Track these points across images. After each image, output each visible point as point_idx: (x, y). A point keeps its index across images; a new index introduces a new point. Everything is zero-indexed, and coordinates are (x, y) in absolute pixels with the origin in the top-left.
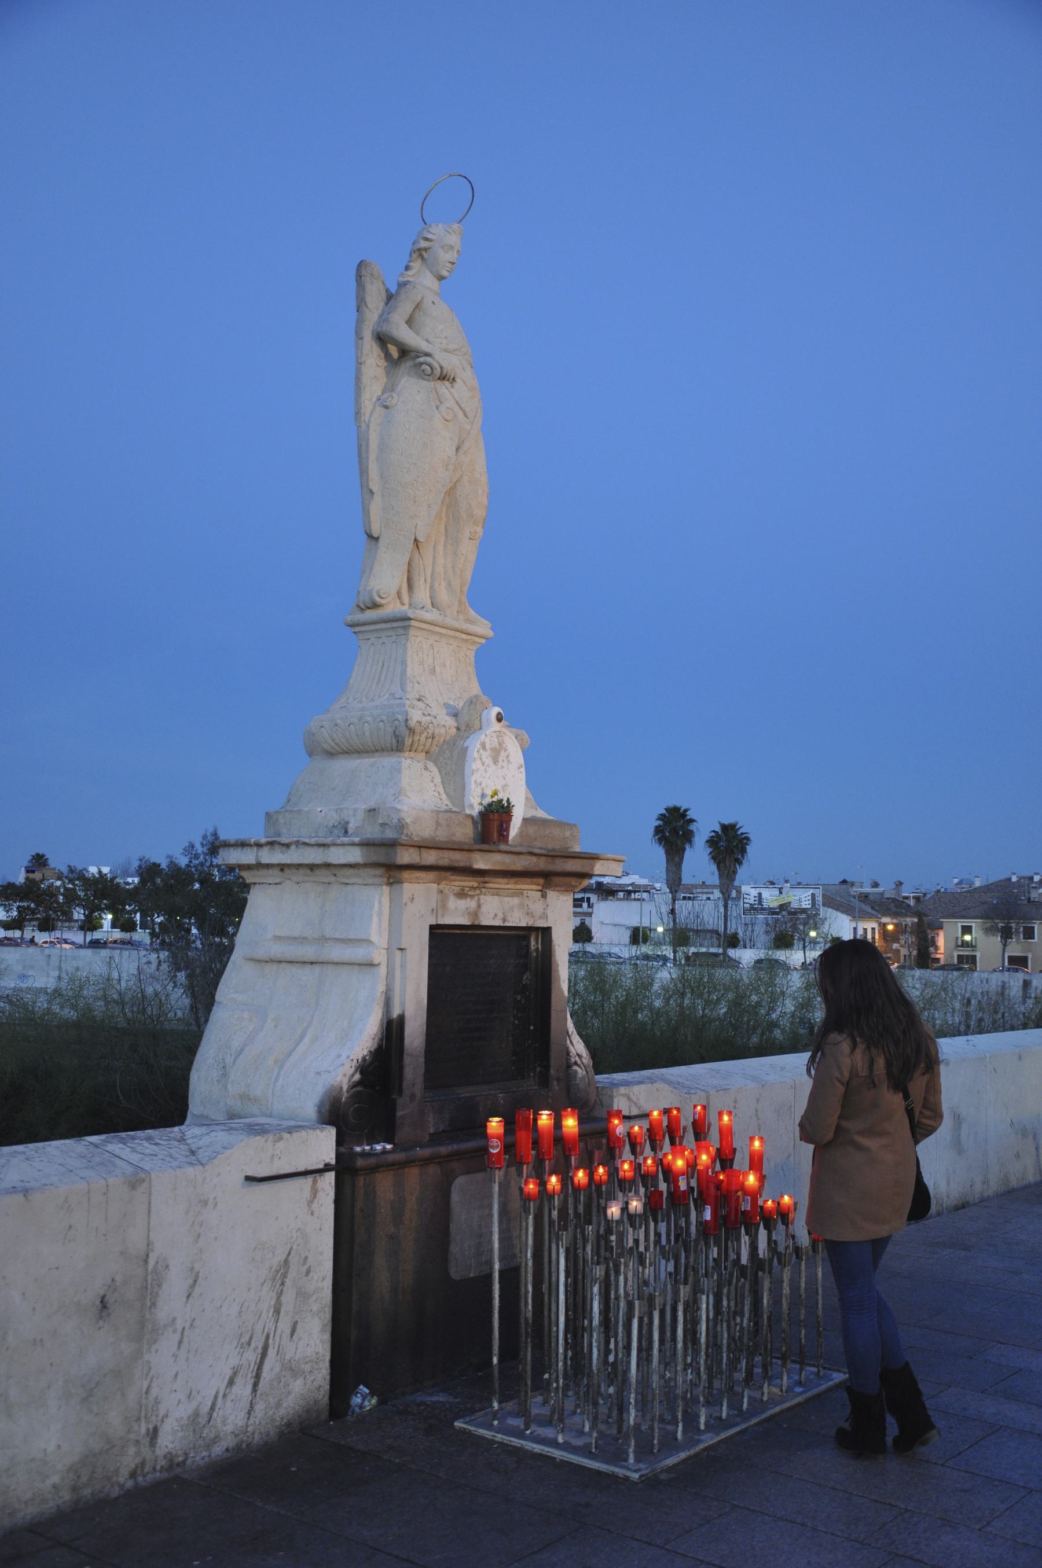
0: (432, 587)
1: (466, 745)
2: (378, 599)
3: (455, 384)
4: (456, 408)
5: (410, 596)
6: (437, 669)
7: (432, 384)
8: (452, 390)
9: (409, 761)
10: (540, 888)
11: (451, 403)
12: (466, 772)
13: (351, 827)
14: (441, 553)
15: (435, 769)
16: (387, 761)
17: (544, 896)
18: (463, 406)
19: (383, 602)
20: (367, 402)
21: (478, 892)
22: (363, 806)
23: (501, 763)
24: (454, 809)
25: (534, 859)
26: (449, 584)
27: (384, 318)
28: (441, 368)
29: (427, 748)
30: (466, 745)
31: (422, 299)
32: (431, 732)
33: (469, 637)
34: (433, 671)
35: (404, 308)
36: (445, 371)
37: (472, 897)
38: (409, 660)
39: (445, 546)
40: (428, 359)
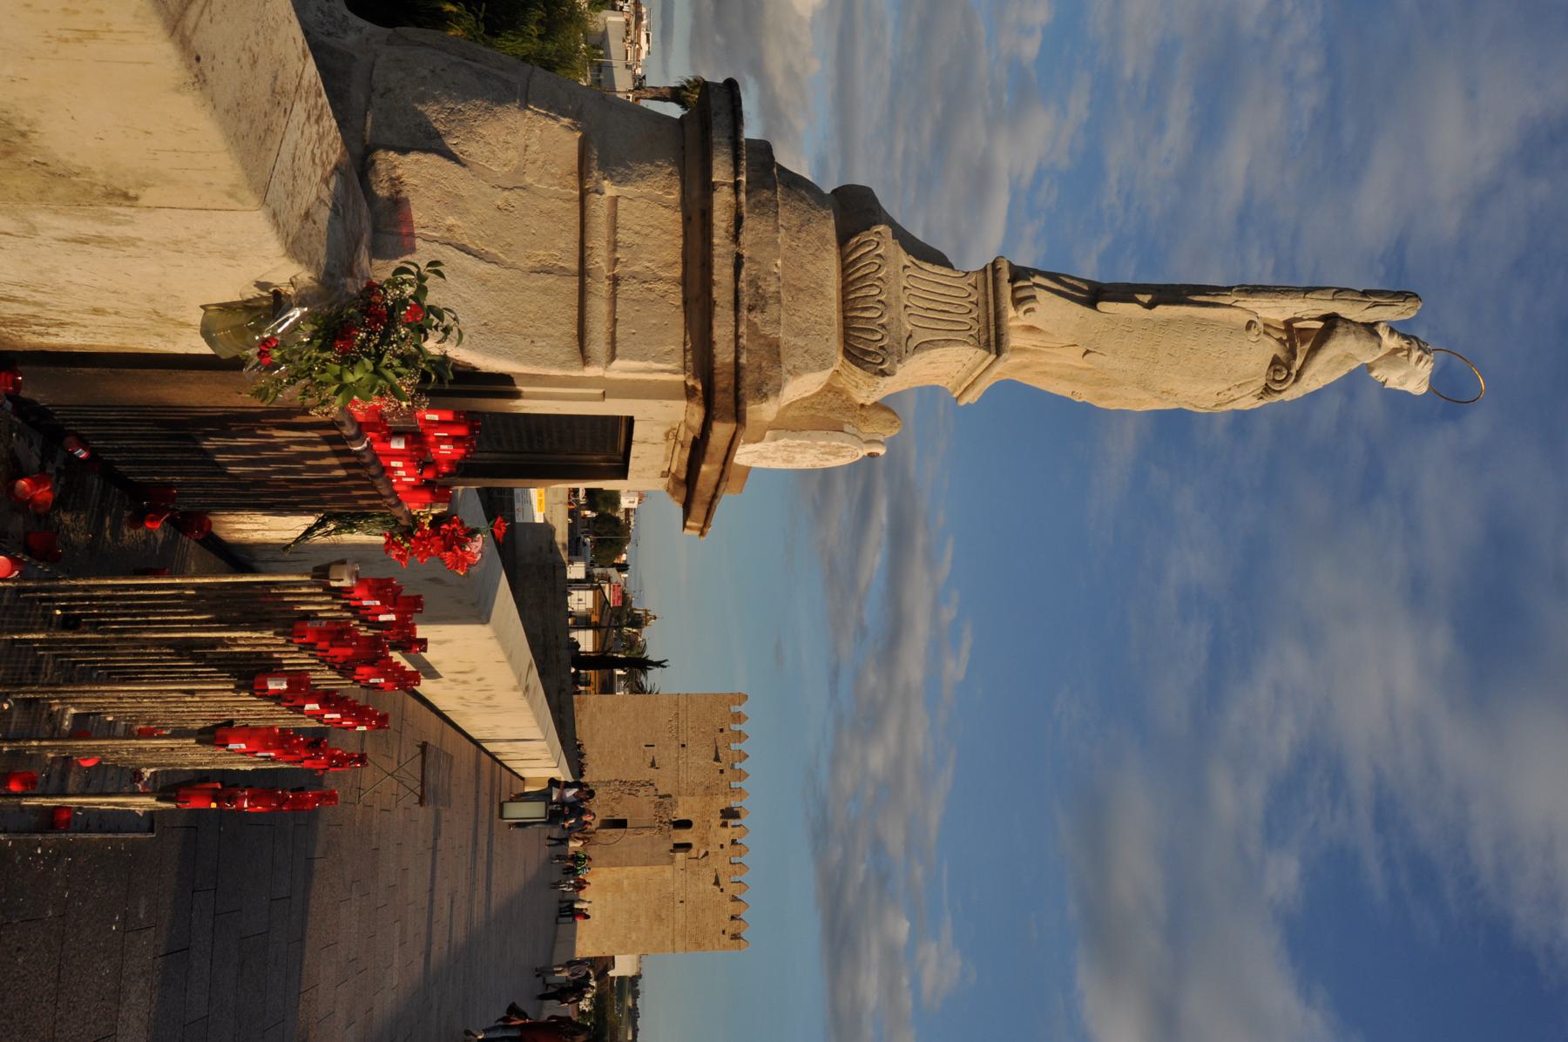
17: (664, 475)
26: (1025, 366)
30: (847, 428)
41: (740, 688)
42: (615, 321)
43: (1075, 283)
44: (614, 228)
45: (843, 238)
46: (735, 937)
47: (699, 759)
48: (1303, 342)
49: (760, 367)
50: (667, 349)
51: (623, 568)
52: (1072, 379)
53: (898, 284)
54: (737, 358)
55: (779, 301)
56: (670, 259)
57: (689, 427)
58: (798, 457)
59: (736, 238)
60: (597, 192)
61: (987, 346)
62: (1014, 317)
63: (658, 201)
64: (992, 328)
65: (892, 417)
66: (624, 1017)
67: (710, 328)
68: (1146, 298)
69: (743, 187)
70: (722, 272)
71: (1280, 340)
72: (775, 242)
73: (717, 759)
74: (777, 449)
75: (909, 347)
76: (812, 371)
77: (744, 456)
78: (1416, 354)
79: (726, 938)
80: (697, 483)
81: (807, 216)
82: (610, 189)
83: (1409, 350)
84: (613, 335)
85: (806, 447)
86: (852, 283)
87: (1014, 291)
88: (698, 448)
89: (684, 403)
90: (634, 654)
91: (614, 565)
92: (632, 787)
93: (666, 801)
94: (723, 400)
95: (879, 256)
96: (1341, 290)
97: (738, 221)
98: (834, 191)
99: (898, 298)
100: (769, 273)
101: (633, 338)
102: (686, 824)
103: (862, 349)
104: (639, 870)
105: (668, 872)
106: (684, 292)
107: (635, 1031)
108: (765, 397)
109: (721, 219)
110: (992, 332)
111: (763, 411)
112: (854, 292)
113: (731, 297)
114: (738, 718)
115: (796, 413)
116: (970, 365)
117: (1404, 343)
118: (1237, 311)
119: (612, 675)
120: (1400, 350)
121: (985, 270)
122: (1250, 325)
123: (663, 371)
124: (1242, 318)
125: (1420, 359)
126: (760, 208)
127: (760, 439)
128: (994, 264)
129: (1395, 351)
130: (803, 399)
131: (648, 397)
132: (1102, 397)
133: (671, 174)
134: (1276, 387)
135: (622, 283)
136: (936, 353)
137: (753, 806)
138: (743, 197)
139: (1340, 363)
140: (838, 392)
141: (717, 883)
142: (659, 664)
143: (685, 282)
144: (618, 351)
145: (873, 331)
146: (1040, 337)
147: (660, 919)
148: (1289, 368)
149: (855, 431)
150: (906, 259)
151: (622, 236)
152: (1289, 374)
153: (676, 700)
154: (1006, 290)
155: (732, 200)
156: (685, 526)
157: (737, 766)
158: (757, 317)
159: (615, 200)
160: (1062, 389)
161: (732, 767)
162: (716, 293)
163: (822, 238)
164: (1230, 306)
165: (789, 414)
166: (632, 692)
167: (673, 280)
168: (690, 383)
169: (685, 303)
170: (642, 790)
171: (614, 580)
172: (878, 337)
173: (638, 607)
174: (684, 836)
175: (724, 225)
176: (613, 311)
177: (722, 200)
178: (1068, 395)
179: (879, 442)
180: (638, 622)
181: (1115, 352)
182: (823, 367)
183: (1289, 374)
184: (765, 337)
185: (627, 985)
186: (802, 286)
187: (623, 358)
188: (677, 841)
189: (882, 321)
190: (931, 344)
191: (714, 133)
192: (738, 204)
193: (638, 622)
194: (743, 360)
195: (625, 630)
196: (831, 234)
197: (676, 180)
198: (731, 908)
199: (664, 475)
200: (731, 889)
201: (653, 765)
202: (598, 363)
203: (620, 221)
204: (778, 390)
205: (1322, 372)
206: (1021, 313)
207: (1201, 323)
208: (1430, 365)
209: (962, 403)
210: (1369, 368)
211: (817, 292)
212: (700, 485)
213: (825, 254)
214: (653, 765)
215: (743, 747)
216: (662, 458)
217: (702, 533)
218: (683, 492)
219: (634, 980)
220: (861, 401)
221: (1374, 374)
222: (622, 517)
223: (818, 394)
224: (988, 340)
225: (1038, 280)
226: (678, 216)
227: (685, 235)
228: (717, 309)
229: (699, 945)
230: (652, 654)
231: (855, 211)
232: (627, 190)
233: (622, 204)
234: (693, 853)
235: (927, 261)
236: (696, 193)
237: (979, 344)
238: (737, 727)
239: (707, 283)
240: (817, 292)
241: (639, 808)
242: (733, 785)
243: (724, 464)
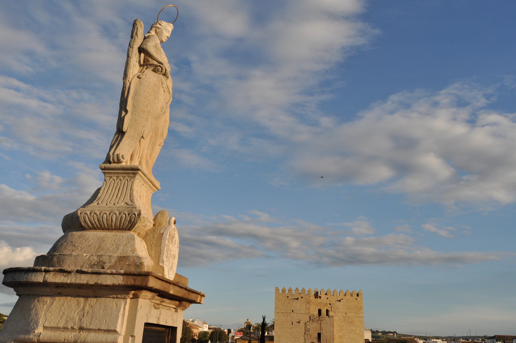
10: (174, 307)
17: (176, 311)
20: (131, 74)
26: (147, 162)
28: (166, 70)
30: (162, 232)
39: (149, 145)
41: (274, 290)
42: (99, 329)
43: (115, 139)
44: (57, 328)
45: (82, 228)
46: (358, 295)
47: (297, 305)
48: (149, 61)
49: (128, 265)
50: (115, 306)
51: (229, 331)
52: (154, 145)
53: (104, 207)
54: (121, 274)
55: (101, 255)
56: (76, 303)
57: (153, 298)
58: (173, 253)
59: (69, 272)
60: (39, 336)
61: (135, 174)
62: (126, 163)
63: (48, 308)
64: (128, 171)
65: (160, 214)
66: (385, 336)
67: (107, 286)
68: (123, 113)
69: (47, 268)
70: (83, 279)
71: (146, 69)
72: (75, 256)
73: (298, 299)
74: (168, 261)
75: (131, 204)
76: (134, 244)
77: (170, 276)
78: (158, 25)
79: (358, 298)
80: (184, 298)
81: (69, 243)
82: (40, 330)
83: (156, 27)
84: (105, 331)
85: (168, 248)
86: (101, 226)
87: (114, 162)
88: (163, 295)
89: (140, 299)
90: (260, 328)
91: (228, 334)
92: (307, 331)
93: (312, 318)
94: (138, 282)
95: (90, 214)
96: (130, 45)
97: (62, 271)
98: (64, 232)
99: (109, 207)
100: (89, 259)
101: (108, 321)
102: (320, 311)
103: (129, 223)
104: (335, 329)
105: (335, 318)
106: (91, 297)
107: (390, 332)
108: (141, 264)
109: (60, 279)
110: (130, 171)
111: (148, 264)
112: (104, 225)
113: (94, 276)
114: (284, 291)
115: (153, 252)
116: (143, 182)
117: (154, 29)
118: (133, 81)
119: (267, 336)
120: (156, 30)
121: (104, 173)
122: (139, 77)
123: (124, 308)
124: (135, 80)
125: (160, 24)
126: (60, 262)
127: (163, 268)
128: (102, 169)
129: (156, 32)
130: (148, 249)
131: (135, 316)
132: (162, 135)
133: (38, 301)
135: (82, 325)
136: (135, 194)
137: (313, 287)
138: (51, 269)
139: (158, 49)
140: (147, 234)
141: (340, 301)
142: (264, 319)
143: (86, 297)
144: (112, 328)
145: (121, 218)
146: (135, 155)
147: (352, 322)
148: (157, 66)
149: (163, 229)
150: (95, 203)
151: (61, 325)
152: (159, 66)
153: (277, 313)
154: (113, 165)
155: (52, 273)
156: (199, 303)
157: (300, 292)
158: (107, 265)
159: (45, 328)
160: (158, 149)
161: (300, 293)
162: (92, 282)
163: (80, 237)
164: (130, 83)
165: (153, 255)
166: (273, 329)
167: (85, 301)
168: (131, 296)
169: (96, 297)
170: (307, 327)
171: (234, 335)
172: (124, 216)
173: (243, 326)
174: (324, 312)
175: (62, 277)
176: (95, 330)
177: (51, 278)
178: (160, 147)
179: (170, 220)
180: (249, 326)
181: (144, 127)
182: (133, 239)
183: (159, 66)
184: (116, 262)
185: (374, 335)
186: (98, 246)
187: (116, 326)
188: (325, 315)
189: (118, 214)
190: (131, 196)
191: (21, 280)
192: (54, 271)
193: (249, 326)
194: (122, 272)
195: (251, 331)
196: (79, 233)
197: (42, 299)
198: (348, 296)
199: (176, 311)
200: (342, 296)
201: (299, 322)
202: (117, 338)
203: (55, 325)
204: (139, 258)
205: (161, 56)
206: (123, 160)
207: (136, 94)
208: (163, 22)
209: (160, 188)
210: (162, 42)
211: (102, 240)
212: (180, 295)
213: (87, 236)
214: (299, 322)
215: (294, 289)
216: (168, 311)
217: (203, 296)
218: (184, 303)
219: (373, 332)
220: (152, 225)
221: (164, 40)
222: (211, 331)
223: (146, 243)
224: (133, 173)
225: (111, 153)
226: (57, 298)
227: (66, 296)
228: (99, 282)
229: (361, 308)
230: (260, 321)
231: (72, 223)
232: (41, 322)
233: (47, 324)
234: (329, 309)
235: (97, 195)
236: (48, 290)
237: (134, 177)
238: (287, 292)
240: (102, 240)
241: (314, 328)
242: (307, 294)
243: (170, 283)
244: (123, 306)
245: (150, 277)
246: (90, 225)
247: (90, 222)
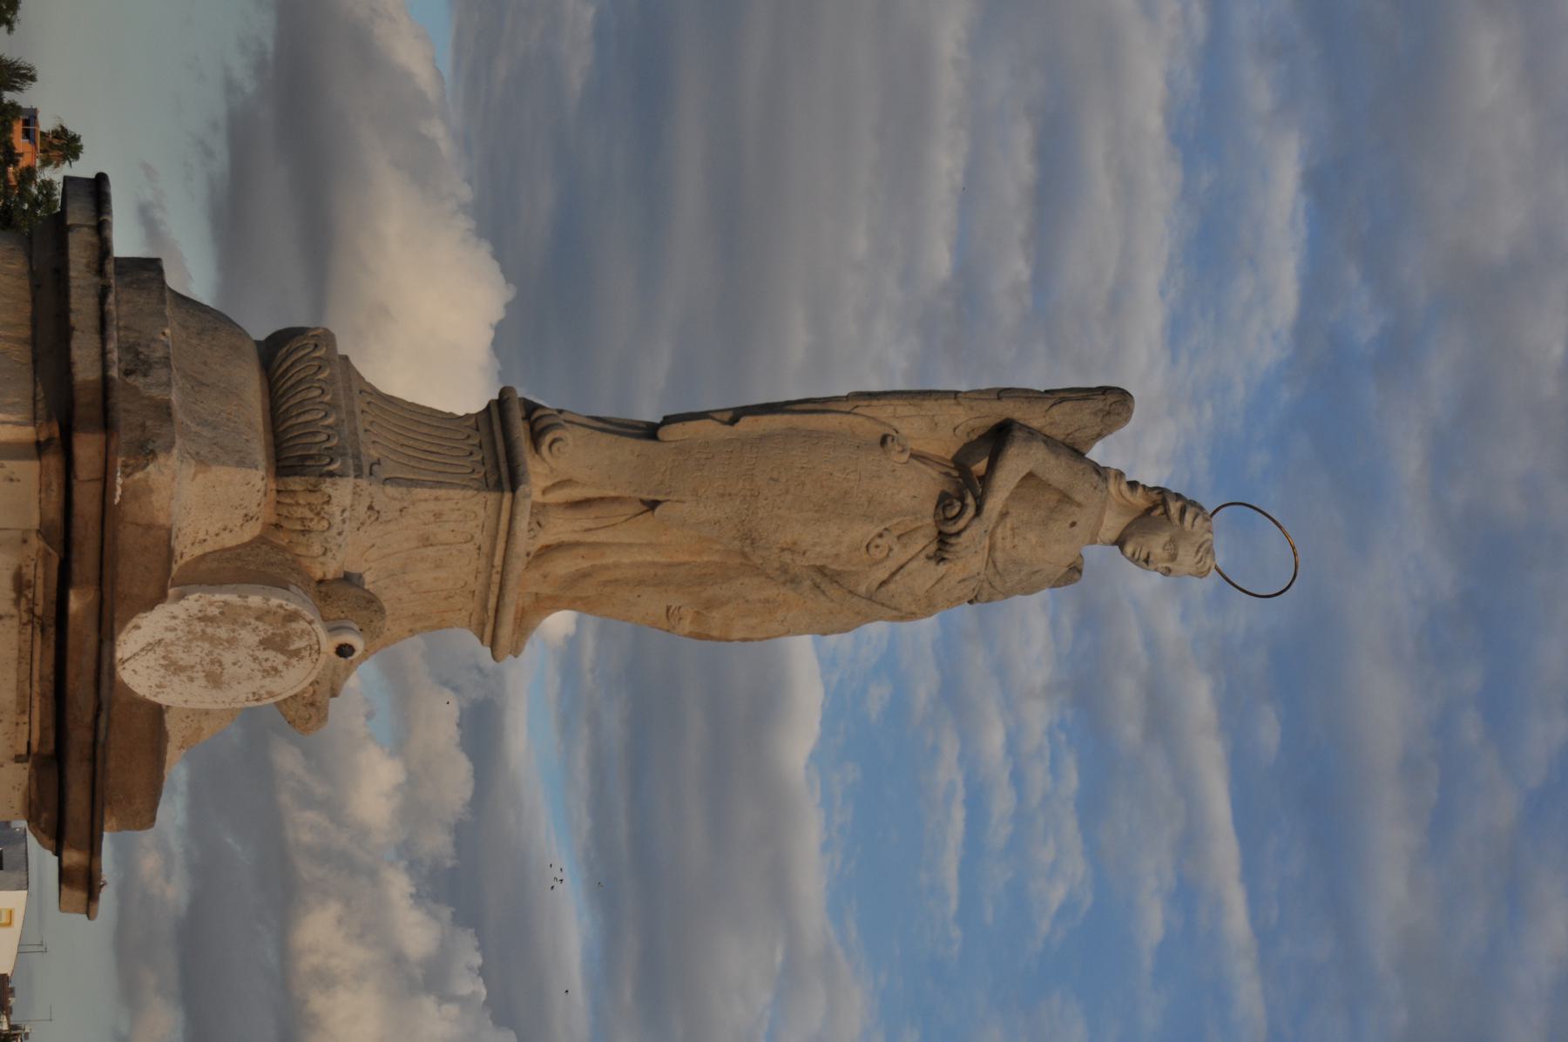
0: (577, 544)
1: (293, 588)
2: (548, 438)
3: (932, 563)
4: (891, 565)
5: (558, 505)
6: (429, 551)
7: (930, 520)
8: (922, 556)
9: (260, 485)
11: (900, 556)
12: (246, 586)
13: (138, 381)
14: (639, 558)
15: (246, 536)
16: (258, 448)
17: (18, 759)
18: (898, 577)
19: (544, 449)
20: (890, 410)
21: (25, 618)
22: (175, 397)
23: (262, 655)
24: (175, 568)
25: (88, 718)
26: (584, 575)
27: (1032, 433)
28: (958, 534)
29: (286, 524)
30: (293, 588)
31: (1079, 505)
32: (313, 525)
33: (491, 613)
34: (426, 541)
35: (1056, 470)
36: (953, 540)
37: (17, 603)
38: (441, 492)
39: (654, 564)
40: (970, 511)
49: (143, 427)
61: (499, 487)
67: (68, 350)
86: (277, 380)
113: (95, 322)
115: (215, 564)
118: (860, 419)
134: (954, 529)
145: (314, 434)
155: (94, 240)
169: (35, 362)
184: (150, 398)
228: (76, 334)
239: (63, 313)
244: (13, 418)
245: (103, 437)
246: (285, 366)
247: (286, 370)
